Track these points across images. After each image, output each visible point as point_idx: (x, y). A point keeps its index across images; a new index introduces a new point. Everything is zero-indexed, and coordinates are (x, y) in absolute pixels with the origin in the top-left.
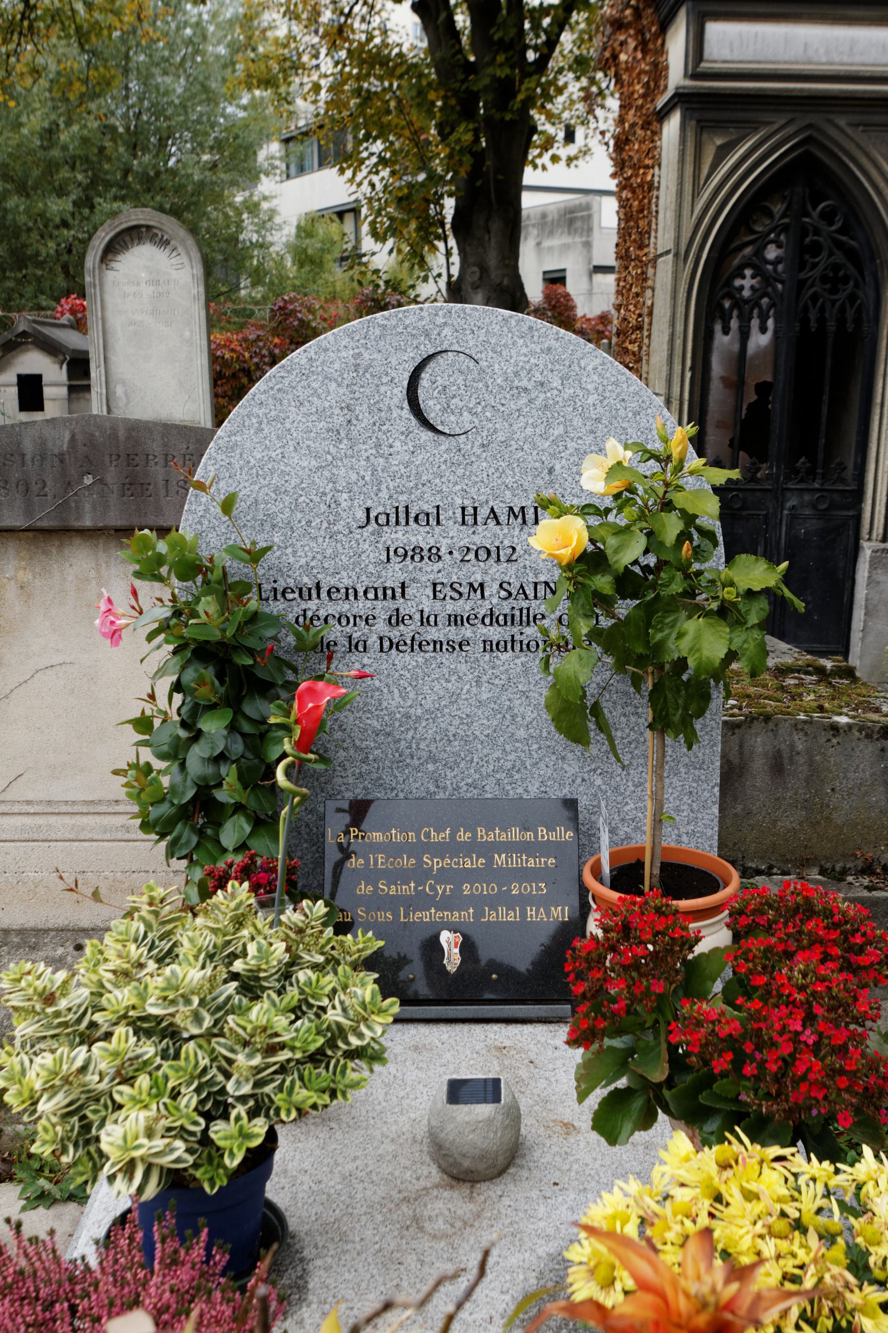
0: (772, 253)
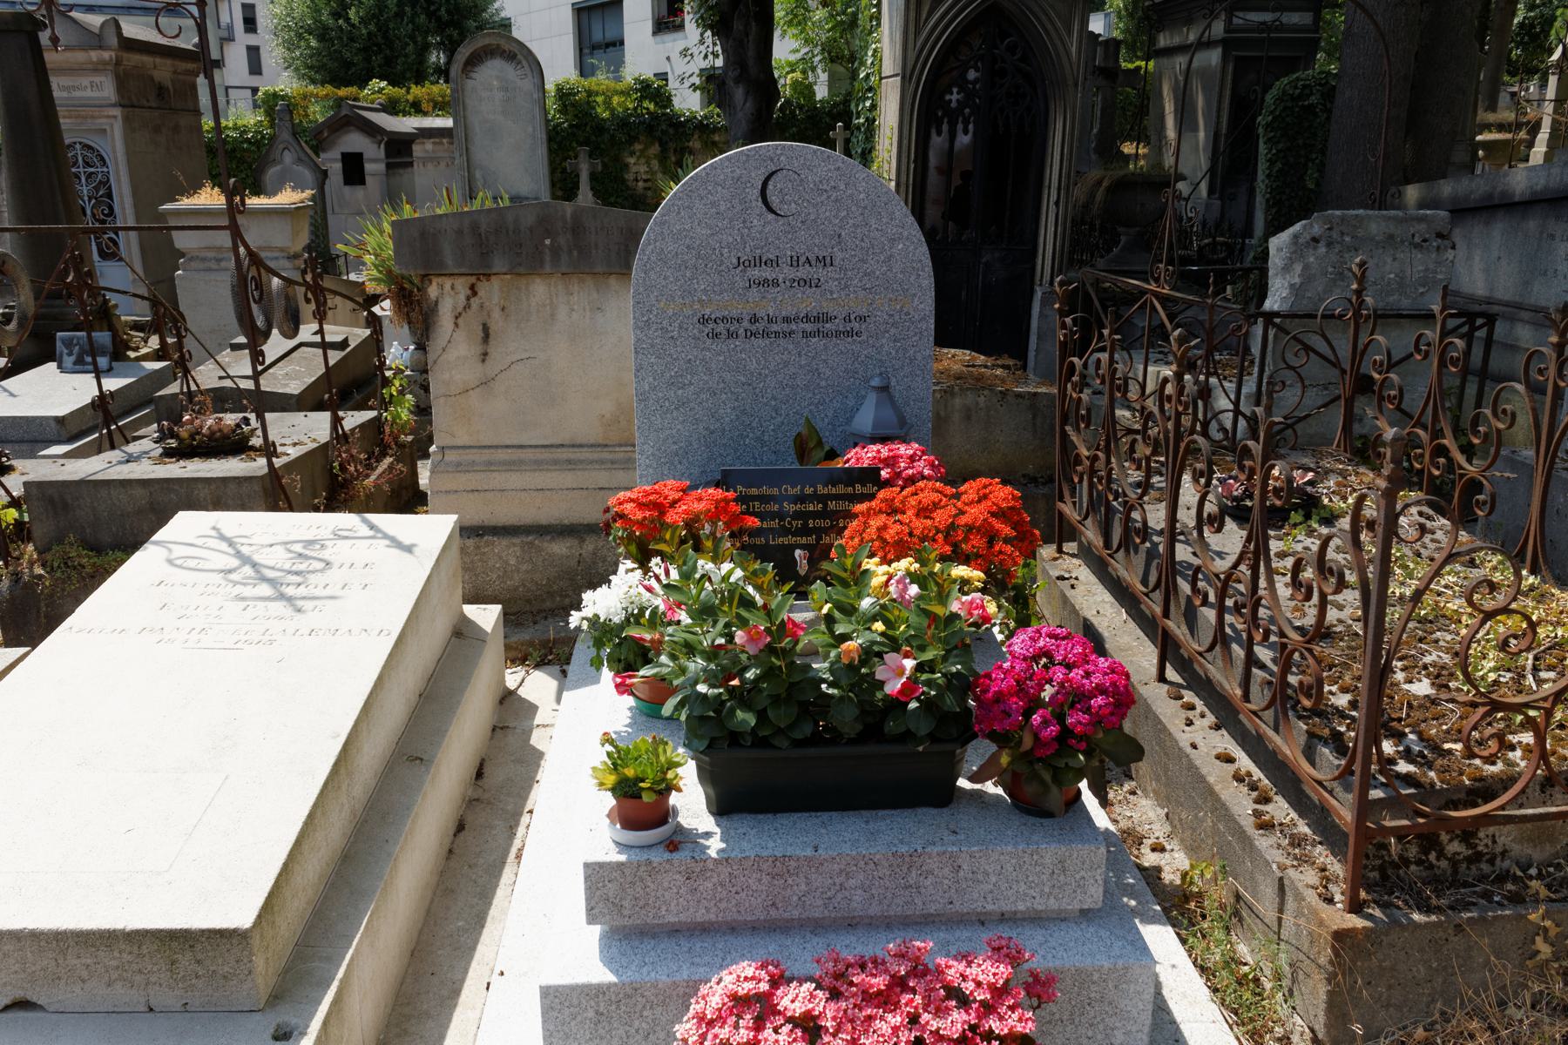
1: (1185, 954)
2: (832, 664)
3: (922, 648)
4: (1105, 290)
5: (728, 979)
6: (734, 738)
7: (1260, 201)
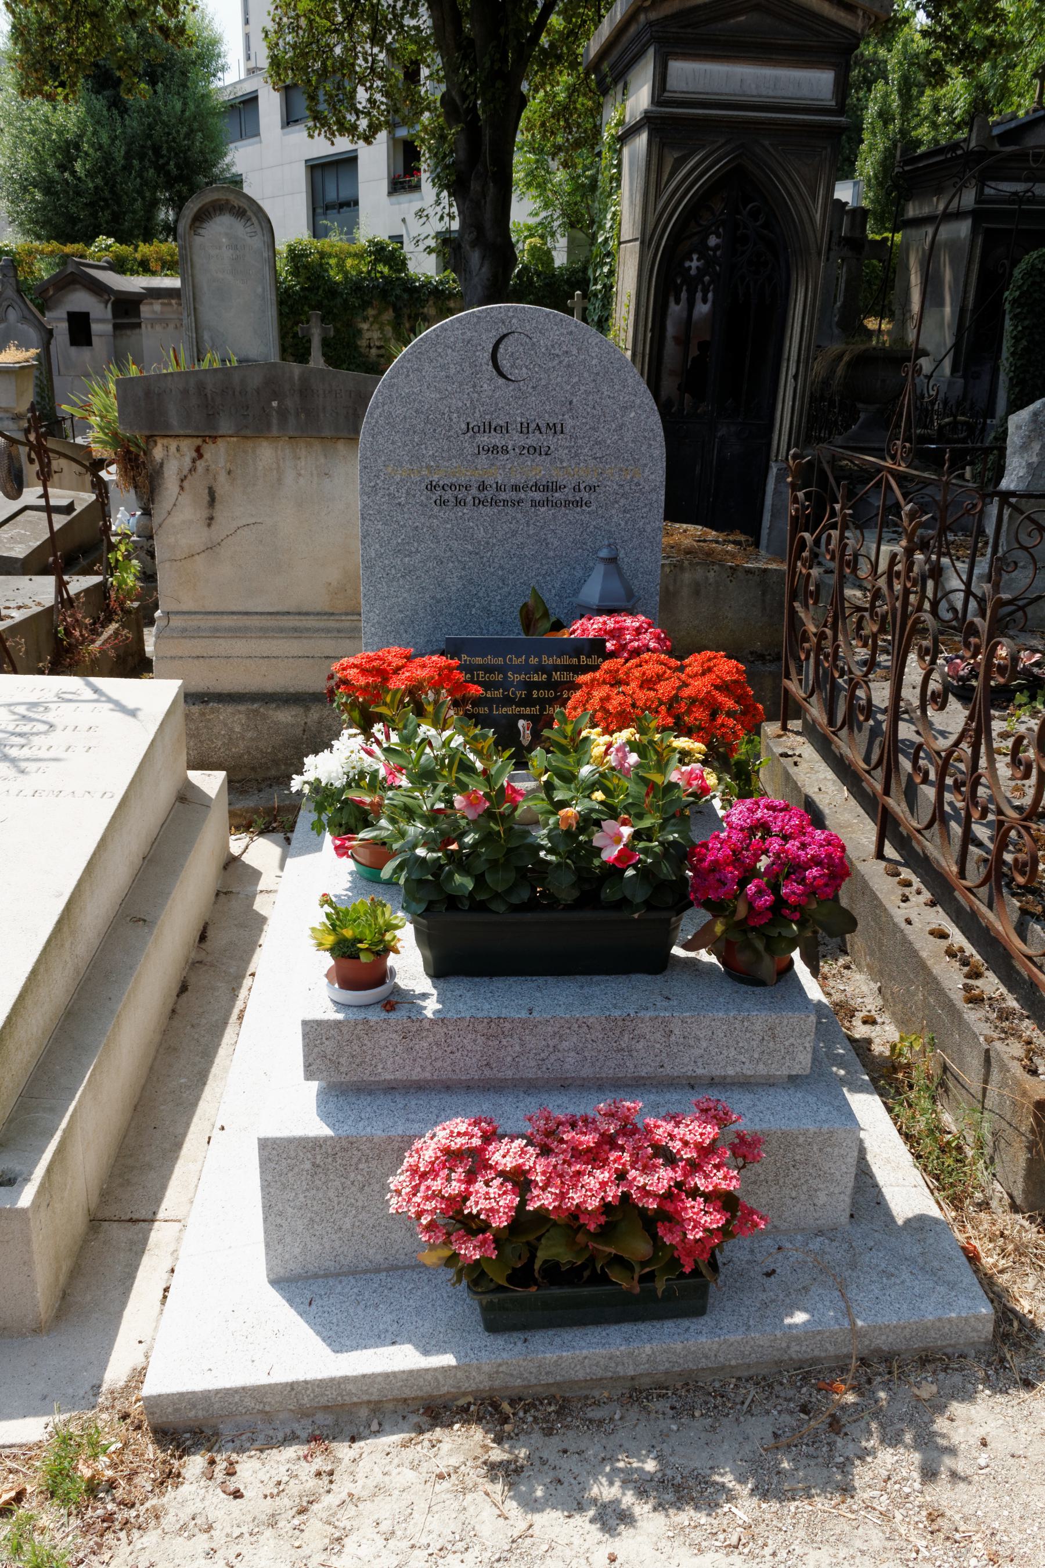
0: (713, 241)
1: (891, 1122)
2: (551, 830)
3: (640, 816)
4: (842, 468)
5: (442, 1134)
6: (452, 902)
7: (1003, 380)
